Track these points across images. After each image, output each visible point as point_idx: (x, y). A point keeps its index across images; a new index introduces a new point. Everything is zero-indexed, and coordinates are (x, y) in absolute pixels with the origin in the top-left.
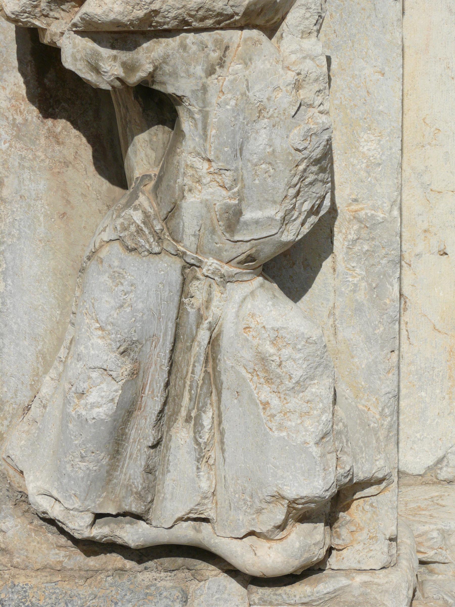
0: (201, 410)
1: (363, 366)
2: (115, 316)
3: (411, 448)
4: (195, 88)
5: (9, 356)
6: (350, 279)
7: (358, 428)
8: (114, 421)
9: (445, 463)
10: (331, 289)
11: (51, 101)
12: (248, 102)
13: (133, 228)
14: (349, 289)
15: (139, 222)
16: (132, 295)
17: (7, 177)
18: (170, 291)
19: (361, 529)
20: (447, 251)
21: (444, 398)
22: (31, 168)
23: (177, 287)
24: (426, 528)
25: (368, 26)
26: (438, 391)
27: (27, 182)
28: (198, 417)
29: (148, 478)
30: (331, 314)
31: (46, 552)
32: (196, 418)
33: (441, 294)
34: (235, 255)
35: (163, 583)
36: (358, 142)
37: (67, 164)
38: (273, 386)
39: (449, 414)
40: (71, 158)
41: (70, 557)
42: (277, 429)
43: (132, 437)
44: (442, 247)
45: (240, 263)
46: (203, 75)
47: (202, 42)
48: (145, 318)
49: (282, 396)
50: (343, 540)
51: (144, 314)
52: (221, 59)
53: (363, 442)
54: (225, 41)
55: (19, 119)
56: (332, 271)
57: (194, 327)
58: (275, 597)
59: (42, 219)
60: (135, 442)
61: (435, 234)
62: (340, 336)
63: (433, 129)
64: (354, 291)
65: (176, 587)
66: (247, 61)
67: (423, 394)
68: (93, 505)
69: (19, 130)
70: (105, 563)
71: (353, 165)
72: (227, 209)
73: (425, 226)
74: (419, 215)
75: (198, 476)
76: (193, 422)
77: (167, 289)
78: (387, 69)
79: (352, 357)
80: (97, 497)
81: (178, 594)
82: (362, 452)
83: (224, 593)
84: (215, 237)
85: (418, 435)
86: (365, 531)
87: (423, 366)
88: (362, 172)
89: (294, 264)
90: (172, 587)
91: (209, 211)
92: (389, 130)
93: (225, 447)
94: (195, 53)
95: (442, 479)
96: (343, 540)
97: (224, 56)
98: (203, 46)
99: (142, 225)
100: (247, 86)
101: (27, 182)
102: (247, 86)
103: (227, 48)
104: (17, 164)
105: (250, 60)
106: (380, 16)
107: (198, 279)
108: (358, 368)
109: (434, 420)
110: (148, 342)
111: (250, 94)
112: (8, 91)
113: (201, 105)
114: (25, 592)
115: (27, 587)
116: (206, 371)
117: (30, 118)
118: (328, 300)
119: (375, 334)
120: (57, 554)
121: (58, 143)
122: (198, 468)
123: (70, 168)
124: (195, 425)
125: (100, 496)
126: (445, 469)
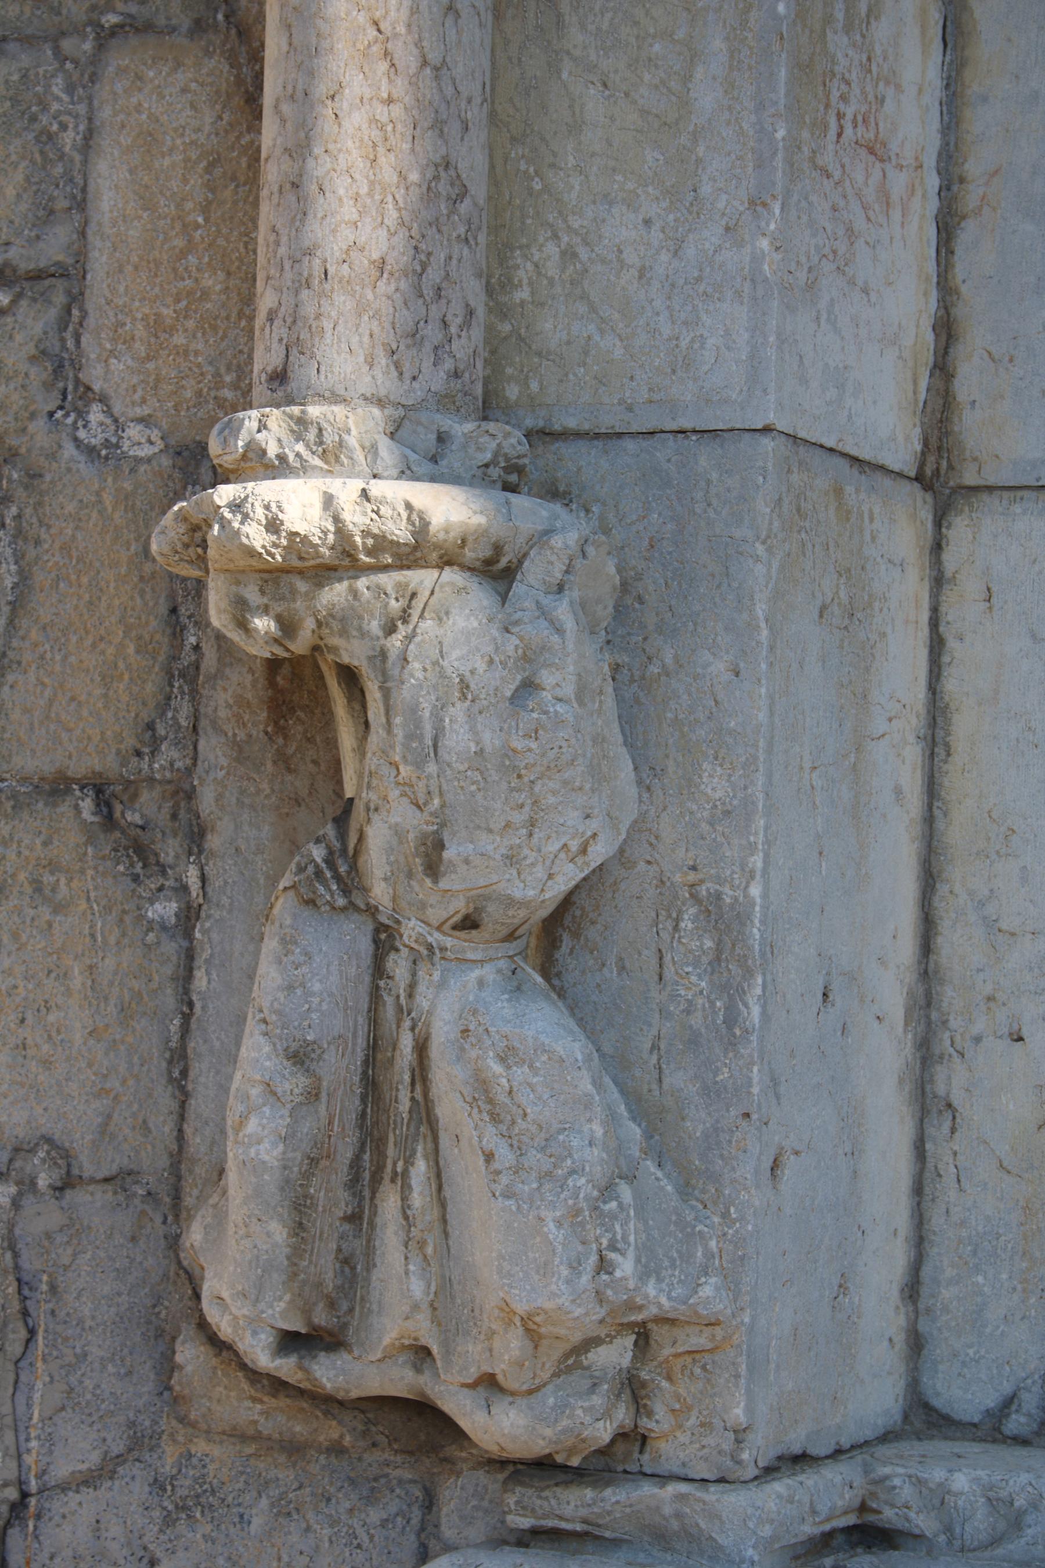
0: (409, 1162)
1: (698, 1134)
2: (282, 999)
3: (959, 1374)
4: (371, 653)
5: (207, 1088)
6: (683, 993)
7: (672, 1228)
8: (285, 1168)
9: (1014, 1407)
10: (654, 1006)
11: (284, 708)
12: (442, 675)
13: (311, 869)
14: (682, 1007)
15: (319, 860)
16: (305, 969)
17: (220, 819)
18: (358, 967)
19: (689, 1409)
20: (1025, 1033)
21: (1014, 1289)
22: (253, 807)
23: (367, 961)
24: (887, 1470)
25: (717, 599)
26: (1004, 1276)
27: (246, 828)
28: (405, 1173)
29: (343, 1272)
30: (655, 1047)
31: (235, 1404)
32: (403, 1174)
33: (1011, 1107)
34: (445, 915)
35: (398, 1472)
36: (700, 777)
37: (298, 802)
38: (501, 1126)
39: (1023, 1318)
40: (304, 792)
41: (266, 1413)
42: (502, 1195)
43: (321, 1203)
44: (1016, 1027)
45: (455, 928)
46: (380, 634)
47: (378, 587)
48: (325, 1006)
49: (515, 1142)
50: (657, 1422)
51: (322, 1001)
52: (404, 611)
53: (678, 1252)
54: (412, 586)
55: (241, 735)
56: (656, 978)
57: (394, 1026)
58: (539, 1502)
59: (262, 881)
60: (324, 1211)
61: (1004, 1004)
62: (667, 1081)
63: (1003, 829)
64: (688, 1012)
65: (415, 1482)
66: (442, 615)
67: (980, 1279)
68: (270, 1312)
69: (241, 751)
70: (316, 1430)
71: (691, 813)
72: (423, 839)
73: (988, 989)
74: (979, 970)
75: (407, 1273)
76: (399, 1183)
77: (354, 963)
78: (742, 665)
79: (683, 1119)
80: (275, 1299)
81: (418, 1493)
82: (673, 1266)
83: (483, 1499)
84: (413, 883)
85: (971, 1352)
86: (695, 1413)
87: (980, 1228)
88: (703, 825)
89: (604, 965)
90: (411, 1481)
91: (401, 843)
92: (743, 759)
93: (449, 1229)
94: (368, 602)
95: (1008, 1433)
96: (657, 1422)
97: (409, 607)
98: (380, 591)
99: (324, 865)
100: (441, 652)
101: (246, 828)
102: (441, 652)
103: (414, 595)
104: (234, 800)
105: (447, 613)
106: (735, 585)
107: (397, 950)
108: (690, 1138)
109: (998, 1327)
110: (332, 1047)
111: (445, 663)
112: (230, 692)
113: (381, 679)
114: (204, 1466)
115: (207, 1460)
116: (413, 1099)
117: (254, 733)
118: (650, 1025)
119: (716, 1083)
120: (250, 1409)
121: (289, 770)
122: (406, 1258)
123: (303, 808)
124: (402, 1187)
125: (280, 1299)
126: (1014, 1416)
